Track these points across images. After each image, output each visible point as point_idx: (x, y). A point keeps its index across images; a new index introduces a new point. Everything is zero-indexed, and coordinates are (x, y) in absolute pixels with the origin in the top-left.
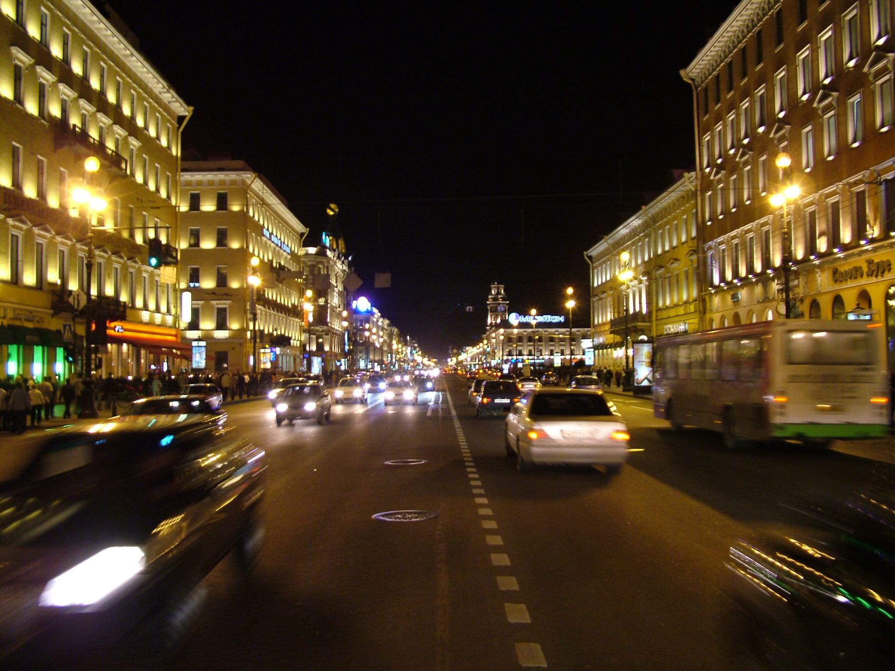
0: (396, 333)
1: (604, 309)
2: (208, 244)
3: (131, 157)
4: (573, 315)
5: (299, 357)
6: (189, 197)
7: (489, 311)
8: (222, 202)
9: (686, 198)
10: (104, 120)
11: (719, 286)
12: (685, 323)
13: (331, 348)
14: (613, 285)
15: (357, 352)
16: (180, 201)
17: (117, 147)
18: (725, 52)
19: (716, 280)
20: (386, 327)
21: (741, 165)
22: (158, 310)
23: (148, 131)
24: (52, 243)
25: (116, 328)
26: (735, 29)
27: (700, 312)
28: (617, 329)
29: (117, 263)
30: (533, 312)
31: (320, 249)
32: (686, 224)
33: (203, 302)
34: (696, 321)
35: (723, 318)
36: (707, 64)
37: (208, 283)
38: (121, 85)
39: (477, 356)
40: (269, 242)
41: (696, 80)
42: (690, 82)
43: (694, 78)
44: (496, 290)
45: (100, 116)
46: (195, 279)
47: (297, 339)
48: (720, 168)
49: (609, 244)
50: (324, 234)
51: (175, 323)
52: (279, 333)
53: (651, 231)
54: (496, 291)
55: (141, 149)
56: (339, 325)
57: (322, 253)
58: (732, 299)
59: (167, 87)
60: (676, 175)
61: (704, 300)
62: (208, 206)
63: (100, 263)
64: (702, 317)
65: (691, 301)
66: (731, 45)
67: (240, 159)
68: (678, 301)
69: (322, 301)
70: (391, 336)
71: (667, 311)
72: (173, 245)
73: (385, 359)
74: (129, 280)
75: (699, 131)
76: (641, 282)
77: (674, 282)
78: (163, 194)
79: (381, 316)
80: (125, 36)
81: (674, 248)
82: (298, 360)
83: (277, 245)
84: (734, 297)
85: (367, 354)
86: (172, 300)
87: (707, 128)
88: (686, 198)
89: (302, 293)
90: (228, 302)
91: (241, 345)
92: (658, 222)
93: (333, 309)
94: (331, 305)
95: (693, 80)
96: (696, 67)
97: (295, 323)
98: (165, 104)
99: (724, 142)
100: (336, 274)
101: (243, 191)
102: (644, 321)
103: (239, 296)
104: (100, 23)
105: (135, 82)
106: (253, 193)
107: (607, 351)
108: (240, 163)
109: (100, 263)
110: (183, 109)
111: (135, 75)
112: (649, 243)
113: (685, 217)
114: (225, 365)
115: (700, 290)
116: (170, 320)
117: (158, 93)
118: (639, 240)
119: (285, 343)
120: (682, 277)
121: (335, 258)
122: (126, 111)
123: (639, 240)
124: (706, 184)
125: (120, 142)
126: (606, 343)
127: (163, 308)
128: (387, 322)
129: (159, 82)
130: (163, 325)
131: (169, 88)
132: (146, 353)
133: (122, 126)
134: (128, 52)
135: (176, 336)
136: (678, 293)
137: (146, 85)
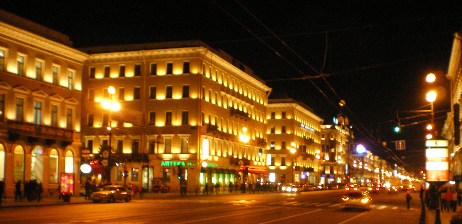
22: (259, 161)
24: (230, 144)
57: (333, 128)
108: (291, 100)
128: (376, 158)
130: (261, 166)
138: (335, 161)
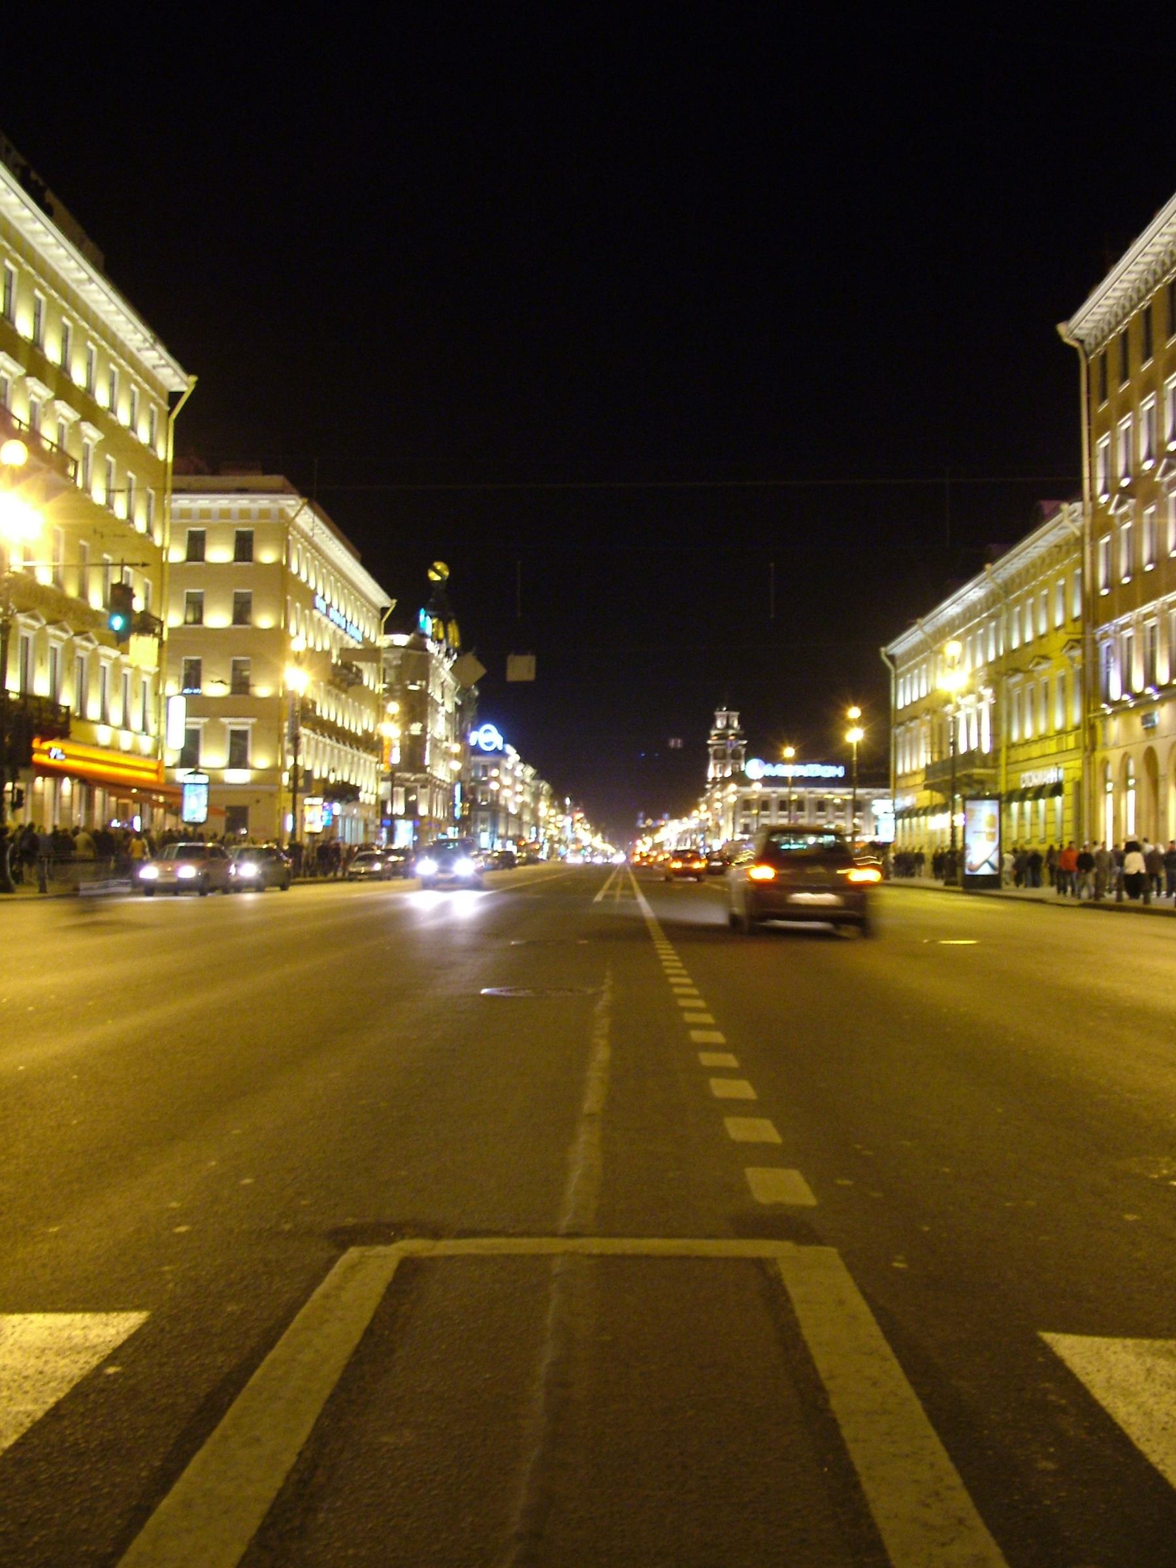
0: (547, 792)
1: (914, 744)
2: (218, 617)
3: (86, 459)
4: (858, 755)
5: (373, 822)
6: (187, 536)
7: (712, 758)
8: (244, 546)
9: (1064, 549)
10: (40, 390)
11: (1119, 702)
12: (1059, 768)
13: (430, 811)
14: (932, 706)
15: (476, 822)
16: (170, 539)
17: (61, 439)
18: (1139, 290)
19: (1115, 693)
20: (528, 780)
21: (1164, 489)
22: (126, 725)
23: (115, 413)
25: (51, 752)
26: (1157, 249)
27: (1086, 749)
28: (937, 780)
29: (57, 637)
30: (789, 752)
31: (414, 638)
32: (1064, 594)
33: (206, 720)
34: (1078, 763)
35: (1126, 757)
36: (1106, 313)
37: (215, 687)
38: (71, 333)
39: (688, 835)
40: (325, 620)
41: (1087, 342)
42: (1075, 344)
43: (1081, 338)
44: (726, 721)
45: (32, 382)
46: (193, 682)
47: (370, 791)
48: (1126, 493)
49: (925, 633)
50: (422, 612)
51: (156, 750)
52: (339, 778)
53: (1000, 609)
54: (725, 722)
55: (103, 446)
56: (443, 770)
57: (418, 645)
58: (1143, 724)
59: (151, 341)
60: (1046, 511)
61: (1092, 728)
62: (220, 553)
63: (27, 639)
64: (1089, 757)
65: (1069, 729)
66: (1151, 279)
67: (278, 473)
68: (1047, 730)
69: (416, 729)
70: (536, 796)
71: (1026, 747)
72: (155, 613)
73: (526, 834)
74: (76, 670)
75: (1089, 430)
76: (980, 699)
77: (1041, 699)
78: (140, 525)
79: (520, 761)
80: (79, 246)
81: (1042, 637)
82: (372, 828)
83: (339, 626)
84: (1147, 720)
85: (495, 825)
86: (151, 706)
87: (1105, 425)
88: (1064, 549)
89: (380, 712)
90: (251, 721)
91: (272, 795)
92: (1013, 593)
93: (436, 743)
94: (432, 736)
95: (1081, 342)
96: (1087, 318)
97: (368, 763)
98: (146, 369)
99: (1134, 451)
100: (442, 683)
101: (282, 530)
102: (985, 766)
103: (270, 710)
104: (47, 236)
105: (95, 327)
106: (298, 533)
107: (918, 822)
108: (277, 480)
109: (27, 639)
110: (177, 380)
111: (97, 317)
112: (997, 629)
113: (1062, 582)
114: (244, 831)
115: (1086, 709)
116: (146, 745)
117: (134, 350)
118: (979, 625)
119: (350, 797)
120: (1055, 687)
121: (441, 655)
122: (79, 377)
123: (979, 625)
124: (1101, 524)
125: (66, 431)
126: (918, 806)
127: (136, 723)
128: (530, 771)
129: (136, 330)
131: (155, 341)
132: (104, 796)
133: (70, 403)
134: (83, 276)
135: (156, 772)
136: (1047, 717)
137: (114, 335)
138: (422, 769)
